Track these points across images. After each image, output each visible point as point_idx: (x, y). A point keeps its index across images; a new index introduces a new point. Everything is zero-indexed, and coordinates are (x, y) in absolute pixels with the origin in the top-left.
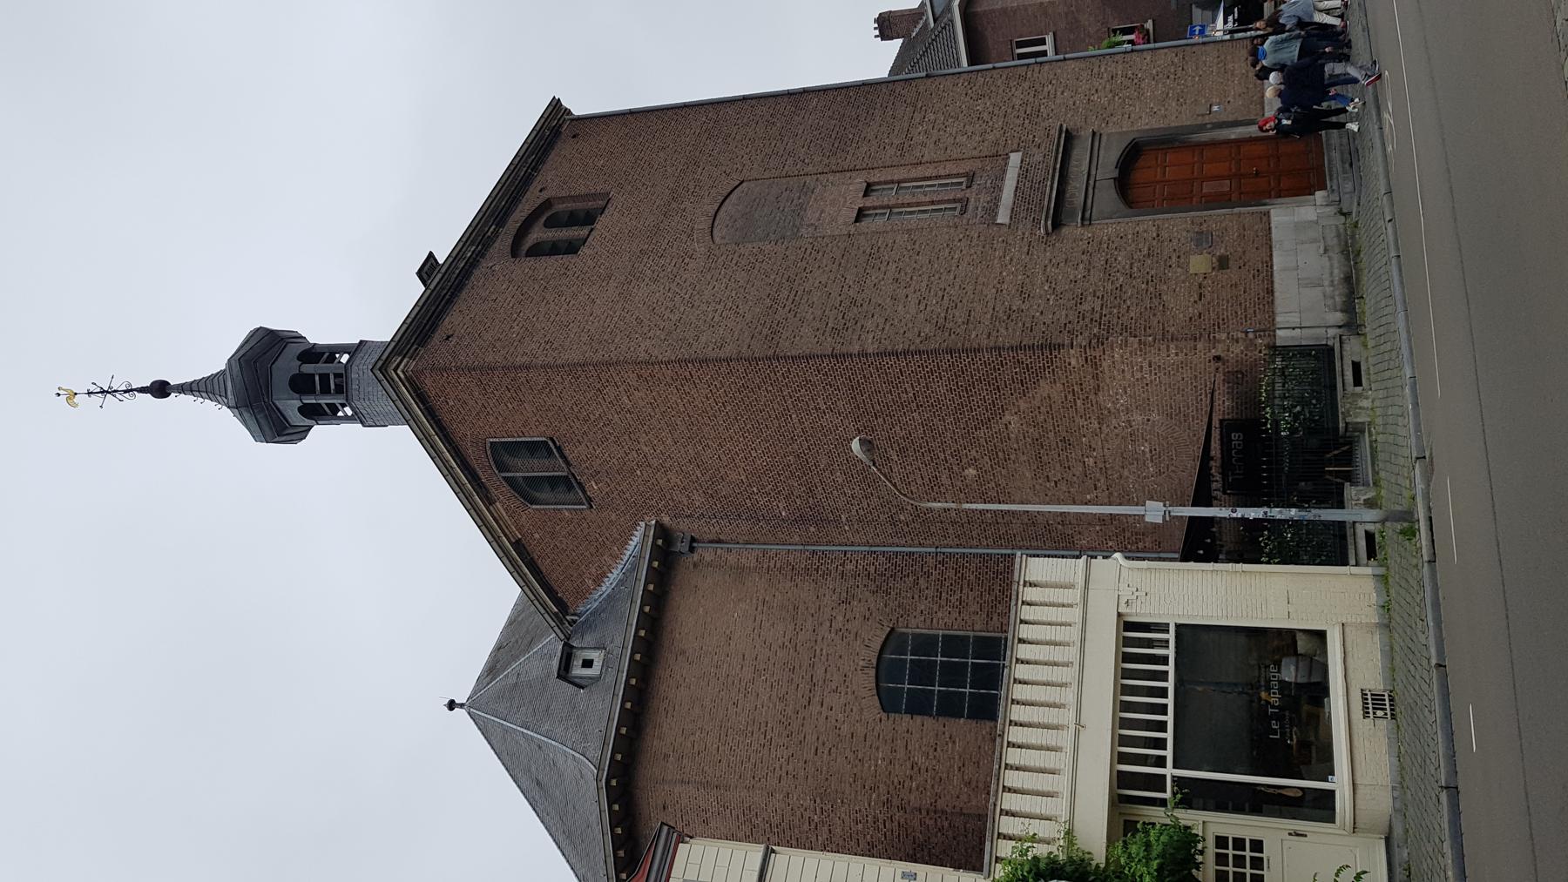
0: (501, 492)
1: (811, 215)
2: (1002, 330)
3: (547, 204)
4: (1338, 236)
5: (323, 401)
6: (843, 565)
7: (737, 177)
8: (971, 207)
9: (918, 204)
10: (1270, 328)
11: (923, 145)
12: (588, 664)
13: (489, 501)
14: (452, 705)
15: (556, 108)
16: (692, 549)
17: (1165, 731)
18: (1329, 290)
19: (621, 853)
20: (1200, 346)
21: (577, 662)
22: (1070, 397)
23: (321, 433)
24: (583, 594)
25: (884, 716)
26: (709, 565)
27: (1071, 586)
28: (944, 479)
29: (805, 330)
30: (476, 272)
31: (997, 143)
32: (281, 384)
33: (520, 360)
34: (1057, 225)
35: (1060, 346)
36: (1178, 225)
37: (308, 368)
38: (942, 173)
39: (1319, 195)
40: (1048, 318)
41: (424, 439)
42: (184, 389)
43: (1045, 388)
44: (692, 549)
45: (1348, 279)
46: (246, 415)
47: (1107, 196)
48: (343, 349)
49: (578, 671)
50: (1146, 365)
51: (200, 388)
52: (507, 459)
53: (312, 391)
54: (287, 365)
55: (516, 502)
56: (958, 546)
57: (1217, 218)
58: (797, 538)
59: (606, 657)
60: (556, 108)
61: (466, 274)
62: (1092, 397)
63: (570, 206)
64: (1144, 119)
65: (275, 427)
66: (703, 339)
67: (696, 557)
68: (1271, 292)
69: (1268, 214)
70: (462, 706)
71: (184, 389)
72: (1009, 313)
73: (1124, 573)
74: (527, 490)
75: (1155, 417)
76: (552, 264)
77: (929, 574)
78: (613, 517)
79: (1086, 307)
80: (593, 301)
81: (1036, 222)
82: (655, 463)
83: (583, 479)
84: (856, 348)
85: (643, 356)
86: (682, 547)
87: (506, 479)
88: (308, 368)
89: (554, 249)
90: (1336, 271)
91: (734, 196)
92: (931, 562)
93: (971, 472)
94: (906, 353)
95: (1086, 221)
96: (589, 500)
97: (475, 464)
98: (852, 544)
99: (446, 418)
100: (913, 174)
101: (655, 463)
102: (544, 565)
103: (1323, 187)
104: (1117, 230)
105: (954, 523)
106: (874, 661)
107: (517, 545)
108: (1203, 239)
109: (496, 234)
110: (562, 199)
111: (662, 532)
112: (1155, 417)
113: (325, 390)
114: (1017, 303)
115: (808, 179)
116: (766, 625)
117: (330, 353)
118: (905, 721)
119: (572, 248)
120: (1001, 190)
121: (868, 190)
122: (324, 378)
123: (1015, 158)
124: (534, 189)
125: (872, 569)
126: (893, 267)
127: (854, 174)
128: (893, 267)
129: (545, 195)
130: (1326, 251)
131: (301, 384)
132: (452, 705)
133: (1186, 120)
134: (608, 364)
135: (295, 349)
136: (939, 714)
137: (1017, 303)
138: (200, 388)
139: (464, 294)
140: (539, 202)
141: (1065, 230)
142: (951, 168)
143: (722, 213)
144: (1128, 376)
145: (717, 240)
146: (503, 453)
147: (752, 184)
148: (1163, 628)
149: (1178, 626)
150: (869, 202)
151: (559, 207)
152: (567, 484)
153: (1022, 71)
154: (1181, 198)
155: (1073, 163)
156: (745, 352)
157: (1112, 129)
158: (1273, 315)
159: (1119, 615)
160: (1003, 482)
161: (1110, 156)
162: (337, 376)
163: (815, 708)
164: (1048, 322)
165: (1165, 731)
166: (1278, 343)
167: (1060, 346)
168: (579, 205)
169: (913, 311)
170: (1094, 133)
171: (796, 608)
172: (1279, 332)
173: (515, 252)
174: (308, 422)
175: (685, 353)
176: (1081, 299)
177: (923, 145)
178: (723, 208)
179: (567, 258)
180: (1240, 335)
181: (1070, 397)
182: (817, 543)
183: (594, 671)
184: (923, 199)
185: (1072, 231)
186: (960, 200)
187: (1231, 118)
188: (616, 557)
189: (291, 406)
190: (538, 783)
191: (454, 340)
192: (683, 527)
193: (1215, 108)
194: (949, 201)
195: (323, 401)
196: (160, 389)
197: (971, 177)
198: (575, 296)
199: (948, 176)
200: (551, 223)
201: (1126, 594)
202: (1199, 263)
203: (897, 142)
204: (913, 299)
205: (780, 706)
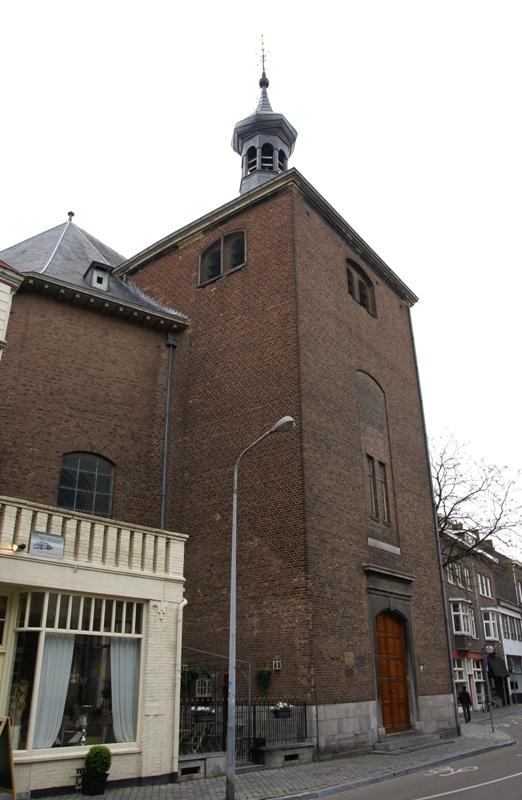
0: (211, 238)
1: (370, 429)
2: (315, 536)
3: (370, 284)
4: (364, 742)
5: (258, 159)
7: (386, 390)
10: (317, 702)
11: (403, 499)
12: (100, 280)
13: (205, 231)
15: (414, 299)
16: (168, 346)
17: (83, 629)
18: (336, 738)
20: (306, 658)
21: (101, 275)
22: (270, 578)
23: (236, 161)
24: (140, 284)
25: (61, 454)
26: (159, 355)
27: (166, 571)
28: (213, 500)
29: (314, 416)
30: (339, 237)
31: (405, 541)
32: (264, 139)
33: (298, 248)
34: (369, 573)
35: (306, 571)
36: (367, 645)
37: (276, 153)
38: (390, 509)
39: (382, 730)
40: (322, 565)
41: (236, 202)
42: (264, 94)
43: (277, 562)
44: (168, 346)
45: (342, 748)
46: (248, 127)
47: (382, 604)
49: (96, 274)
50: (293, 625)
51: (265, 102)
52: (233, 241)
53: (263, 154)
54: (279, 145)
55: (203, 245)
56: (166, 510)
57: (371, 668)
58: (173, 409)
59: (102, 286)
60: (414, 299)
62: (270, 592)
63: (369, 296)
64: (416, 626)
65: (244, 134)
66: (309, 354)
67: (163, 348)
68: (335, 702)
69: (373, 699)
71: (264, 94)
72: (324, 541)
73: (175, 606)
74: (211, 254)
75: (256, 632)
76: (344, 279)
77: (148, 490)
78: (191, 301)
79: (327, 588)
81: (368, 561)
82: (227, 324)
83: (217, 283)
84: (306, 445)
85: (301, 317)
87: (216, 246)
88: (276, 153)
89: (350, 283)
90: (346, 742)
92: (157, 492)
93: (218, 517)
94: (303, 475)
95: (370, 590)
96: (203, 287)
97: (231, 222)
98: (168, 444)
99: (260, 208)
100: (389, 491)
101: (227, 324)
102: (161, 262)
103: (387, 731)
104: (363, 610)
105: (182, 506)
106: (95, 451)
107: (175, 247)
108: (361, 660)
109: (357, 253)
111: (180, 329)
112: (256, 632)
113: (264, 161)
114: (329, 547)
116: (120, 386)
118: (56, 468)
119: (351, 292)
121: (382, 464)
122: (271, 161)
123: (397, 551)
129: (374, 284)
130: (357, 735)
131: (268, 149)
132: (71, 214)
133: (417, 651)
134: (296, 297)
136: (61, 491)
137: (329, 547)
138: (265, 102)
139: (329, 228)
141: (365, 577)
142: (392, 513)
144: (285, 614)
146: (237, 241)
148: (138, 631)
149: (139, 640)
150: (376, 464)
151: (368, 290)
152: (215, 271)
154: (380, 646)
155: (384, 581)
156: (303, 378)
157: (412, 608)
158: (324, 703)
159: (148, 601)
160: (210, 537)
161: (397, 605)
163: (68, 411)
164: (320, 565)
165: (83, 629)
166: (308, 707)
167: (306, 571)
169: (326, 482)
170: (410, 597)
171: (131, 405)
172: (314, 707)
173: (349, 261)
174: (244, 152)
175: (302, 342)
176: (332, 586)
177: (403, 499)
179: (347, 290)
180: (313, 683)
181: (270, 578)
182: (170, 422)
183: (95, 284)
185: (363, 583)
186: (377, 517)
187: (418, 677)
188: (164, 302)
189: (256, 142)
190: (24, 252)
192: (184, 342)
193: (422, 667)
194: (377, 510)
195: (258, 159)
196: (264, 83)
197: (388, 524)
198: (329, 287)
199: (388, 511)
201: (162, 606)
202: (350, 658)
204: (331, 483)
205: (70, 389)
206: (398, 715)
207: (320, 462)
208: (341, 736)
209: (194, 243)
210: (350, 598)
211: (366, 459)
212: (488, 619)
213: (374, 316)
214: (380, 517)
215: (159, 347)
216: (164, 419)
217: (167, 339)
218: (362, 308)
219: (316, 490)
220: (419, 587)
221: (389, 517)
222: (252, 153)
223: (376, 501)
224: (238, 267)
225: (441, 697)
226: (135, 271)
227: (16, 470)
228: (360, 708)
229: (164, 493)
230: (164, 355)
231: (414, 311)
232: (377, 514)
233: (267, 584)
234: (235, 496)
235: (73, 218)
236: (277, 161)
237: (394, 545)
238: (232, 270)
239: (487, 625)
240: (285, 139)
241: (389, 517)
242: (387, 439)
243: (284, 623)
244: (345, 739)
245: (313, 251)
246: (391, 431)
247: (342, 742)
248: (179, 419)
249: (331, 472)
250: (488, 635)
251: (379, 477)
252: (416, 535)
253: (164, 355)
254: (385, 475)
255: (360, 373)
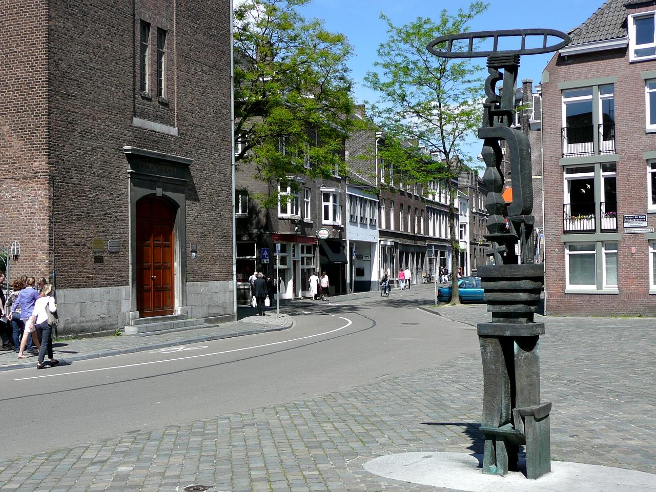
43: (17, 144)
50: (33, 210)
62: (11, 175)
68: (78, 286)
79: (74, 174)
90: (89, 324)
144: (26, 199)
176: (81, 171)
206: (153, 299)
207: (71, 33)
208: (83, 319)
210: (104, 183)
212: (328, 201)
219: (64, 65)
220: (201, 171)
225: (217, 283)
228: (109, 293)
233: (7, 166)
239: (326, 208)
243: (23, 208)
244: (87, 322)
247: (85, 324)
249: (87, 44)
250: (327, 218)
252: (202, 113)
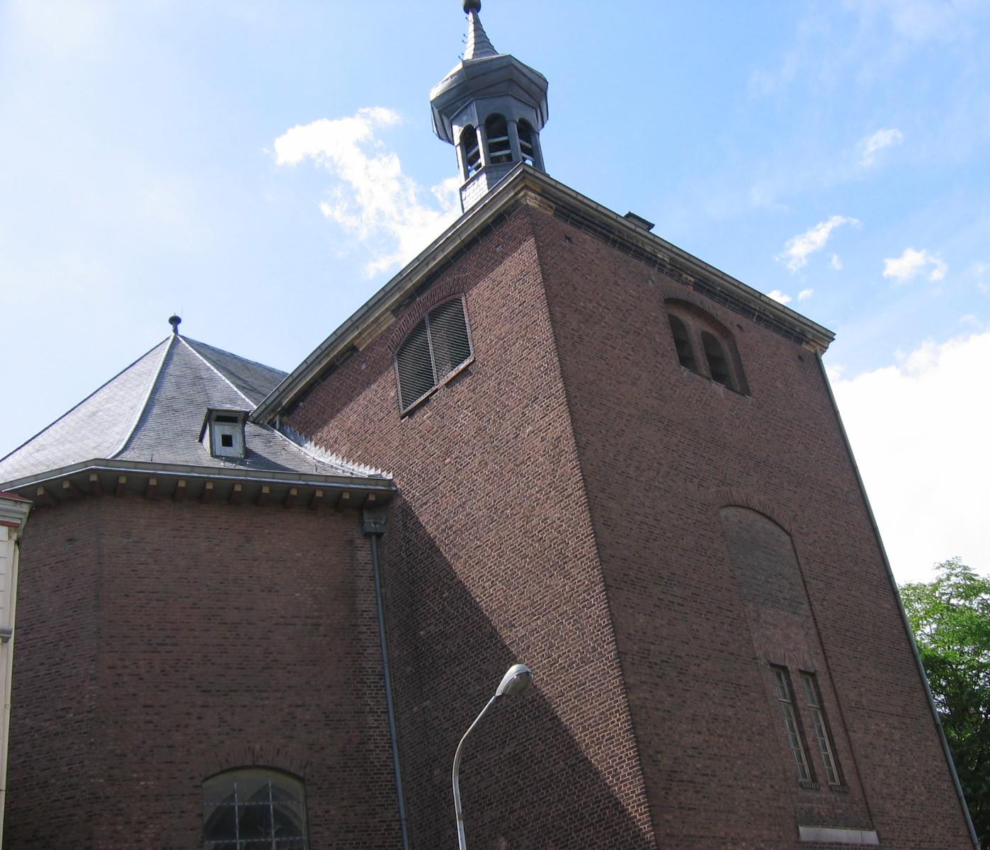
6: (372, 711)
8: (809, 794)
9: (802, 734)
13: (396, 310)
14: (175, 321)
15: (826, 337)
16: (368, 535)
19: (450, 832)
32: (494, 107)
37: (513, 129)
38: (841, 757)
42: (477, 22)
44: (368, 535)
48: (538, 163)
53: (488, 135)
54: (518, 112)
60: (826, 337)
61: (640, 254)
63: (729, 357)
67: (359, 542)
70: (176, 331)
76: (666, 341)
80: (634, 384)
86: (371, 524)
88: (513, 129)
89: (681, 343)
91: (771, 527)
97: (435, 286)
98: (397, 719)
106: (261, 762)
107: (352, 348)
110: (734, 348)
113: (491, 148)
115: (806, 606)
117: (533, 151)
119: (686, 360)
120: (835, 826)
121: (811, 675)
122: (505, 145)
123: (871, 837)
124: (738, 319)
125: (372, 747)
126: (730, 712)
127: (821, 657)
128: (730, 712)
129: (735, 331)
132: (175, 321)
135: (530, 116)
140: (728, 325)
142: (847, 765)
143: (752, 516)
145: (723, 513)
147: (789, 546)
153: (963, 831)
162: (509, 157)
168: (731, 367)
173: (671, 301)
178: (757, 516)
179: (675, 360)
184: (809, 739)
186: (814, 779)
191: (566, 244)
200: (706, 337)
203: (864, 701)
209: (381, 336)
211: (771, 675)
213: (745, 391)
214: (821, 779)
215: (351, 542)
216: (382, 676)
217: (362, 523)
218: (720, 389)
221: (841, 775)
222: (468, 140)
223: (807, 750)
224: (462, 366)
226: (293, 405)
227: (120, 828)
229: (403, 816)
230: (363, 555)
231: (832, 362)
232: (813, 775)
234: (460, 825)
235: (180, 326)
236: (517, 142)
237: (863, 828)
238: (453, 374)
240: (526, 97)
241: (841, 775)
242: (811, 623)
245: (590, 306)
246: (817, 607)
248: (409, 669)
251: (806, 701)
253: (363, 555)
254: (819, 695)
255: (731, 512)
